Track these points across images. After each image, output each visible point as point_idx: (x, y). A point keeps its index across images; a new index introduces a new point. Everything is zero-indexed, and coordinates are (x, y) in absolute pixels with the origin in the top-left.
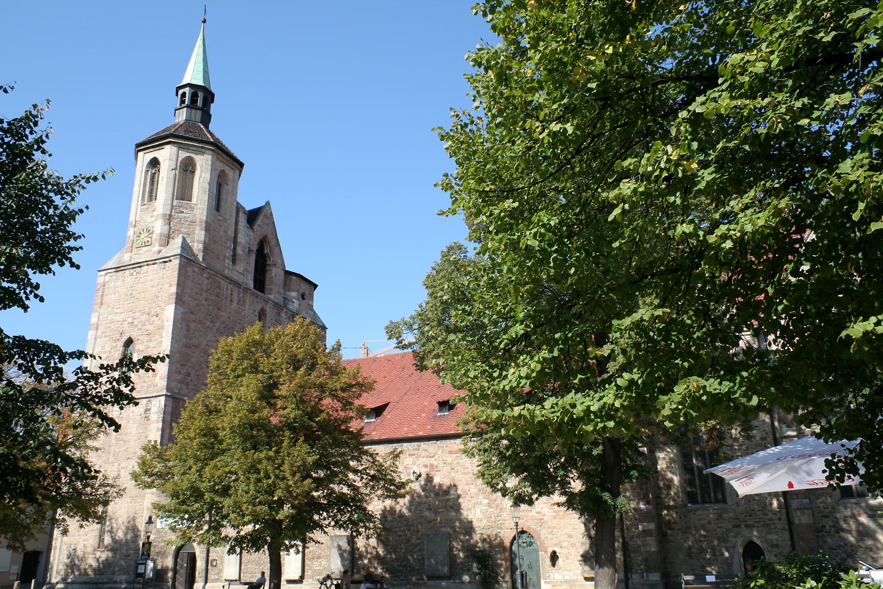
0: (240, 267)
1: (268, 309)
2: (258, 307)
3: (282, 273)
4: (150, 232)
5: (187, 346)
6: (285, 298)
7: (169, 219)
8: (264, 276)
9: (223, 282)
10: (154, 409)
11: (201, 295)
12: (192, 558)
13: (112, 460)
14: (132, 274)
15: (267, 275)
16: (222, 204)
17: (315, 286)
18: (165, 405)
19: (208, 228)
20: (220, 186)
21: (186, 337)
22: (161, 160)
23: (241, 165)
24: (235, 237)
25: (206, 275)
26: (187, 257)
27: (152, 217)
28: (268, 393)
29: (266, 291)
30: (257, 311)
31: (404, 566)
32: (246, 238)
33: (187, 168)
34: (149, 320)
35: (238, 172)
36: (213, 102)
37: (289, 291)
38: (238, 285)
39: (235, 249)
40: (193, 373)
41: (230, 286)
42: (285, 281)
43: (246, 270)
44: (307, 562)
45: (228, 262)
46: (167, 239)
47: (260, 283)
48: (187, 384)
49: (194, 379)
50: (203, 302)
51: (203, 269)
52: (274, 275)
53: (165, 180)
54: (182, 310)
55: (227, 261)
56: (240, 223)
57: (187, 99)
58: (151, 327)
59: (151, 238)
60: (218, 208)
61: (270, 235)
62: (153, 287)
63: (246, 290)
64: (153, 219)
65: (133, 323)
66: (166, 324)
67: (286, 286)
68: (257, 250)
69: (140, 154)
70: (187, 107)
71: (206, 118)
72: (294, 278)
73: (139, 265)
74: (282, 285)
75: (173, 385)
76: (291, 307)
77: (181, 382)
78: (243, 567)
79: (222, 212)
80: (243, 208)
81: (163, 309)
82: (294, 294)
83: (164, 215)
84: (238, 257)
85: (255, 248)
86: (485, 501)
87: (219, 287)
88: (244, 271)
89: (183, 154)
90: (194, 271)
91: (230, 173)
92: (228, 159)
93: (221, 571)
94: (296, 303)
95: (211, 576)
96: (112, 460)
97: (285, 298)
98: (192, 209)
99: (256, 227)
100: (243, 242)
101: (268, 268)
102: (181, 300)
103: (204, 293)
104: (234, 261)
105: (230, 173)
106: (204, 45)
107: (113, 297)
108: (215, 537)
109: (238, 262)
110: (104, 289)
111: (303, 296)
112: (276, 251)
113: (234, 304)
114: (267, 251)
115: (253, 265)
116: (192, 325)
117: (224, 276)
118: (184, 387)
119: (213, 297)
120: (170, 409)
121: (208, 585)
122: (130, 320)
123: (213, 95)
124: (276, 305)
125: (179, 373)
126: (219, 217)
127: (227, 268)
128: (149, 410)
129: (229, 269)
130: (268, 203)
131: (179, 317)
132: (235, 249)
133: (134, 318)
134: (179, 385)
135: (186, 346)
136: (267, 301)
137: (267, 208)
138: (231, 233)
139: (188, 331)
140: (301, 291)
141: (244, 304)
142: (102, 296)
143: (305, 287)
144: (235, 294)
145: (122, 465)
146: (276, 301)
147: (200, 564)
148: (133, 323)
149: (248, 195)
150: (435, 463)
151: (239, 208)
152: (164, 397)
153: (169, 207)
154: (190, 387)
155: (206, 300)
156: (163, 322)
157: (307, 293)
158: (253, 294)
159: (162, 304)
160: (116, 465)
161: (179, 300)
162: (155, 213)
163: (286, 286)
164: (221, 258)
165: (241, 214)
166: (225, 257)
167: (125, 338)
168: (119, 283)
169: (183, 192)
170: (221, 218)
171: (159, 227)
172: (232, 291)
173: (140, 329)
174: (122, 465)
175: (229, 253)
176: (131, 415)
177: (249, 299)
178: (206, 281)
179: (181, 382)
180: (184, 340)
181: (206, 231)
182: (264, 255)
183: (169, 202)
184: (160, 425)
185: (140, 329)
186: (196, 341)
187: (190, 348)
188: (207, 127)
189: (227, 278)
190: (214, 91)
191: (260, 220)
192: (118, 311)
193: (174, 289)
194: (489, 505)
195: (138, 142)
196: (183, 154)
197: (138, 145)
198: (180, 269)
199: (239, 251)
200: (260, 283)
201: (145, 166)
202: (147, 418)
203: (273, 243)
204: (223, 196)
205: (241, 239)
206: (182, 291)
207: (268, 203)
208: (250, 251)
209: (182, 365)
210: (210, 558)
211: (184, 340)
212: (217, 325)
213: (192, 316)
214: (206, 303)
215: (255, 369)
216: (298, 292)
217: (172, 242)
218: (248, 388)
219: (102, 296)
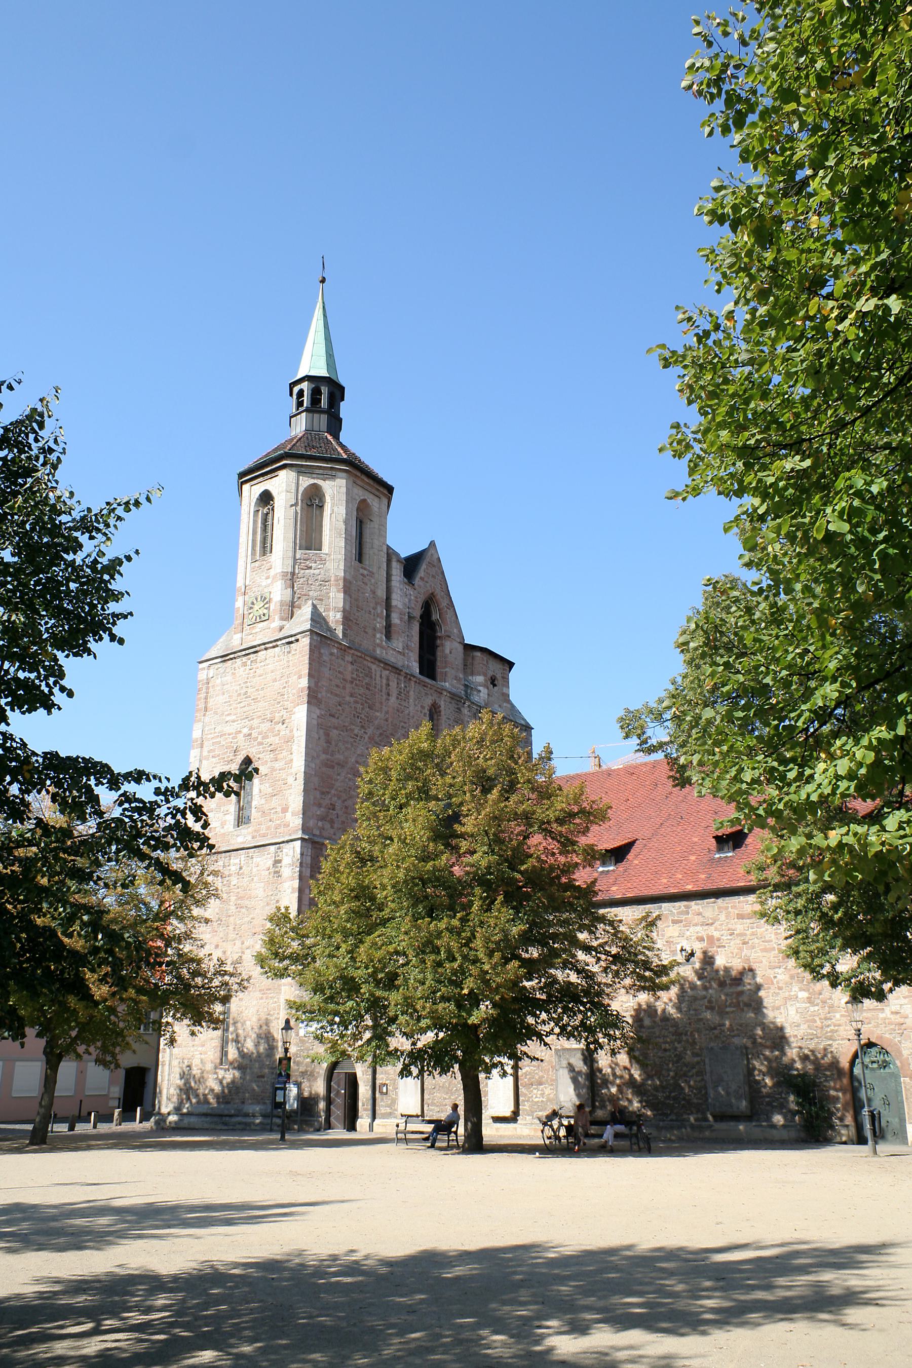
0: (398, 643)
1: (442, 704)
2: (428, 701)
3: (460, 648)
4: (266, 601)
5: (329, 764)
6: (466, 686)
7: (291, 578)
8: (434, 654)
9: (374, 667)
10: (286, 861)
11: (344, 688)
12: (352, 1082)
13: (232, 936)
14: (244, 664)
15: (439, 653)
16: (367, 550)
17: (511, 665)
18: (302, 854)
19: (347, 589)
20: (360, 524)
21: (325, 752)
22: (274, 493)
23: (390, 489)
24: (388, 599)
25: (349, 658)
26: (320, 634)
27: (268, 578)
28: (446, 830)
29: (438, 677)
30: (427, 708)
31: (675, 1098)
32: (404, 599)
33: (312, 501)
34: (272, 730)
35: (385, 501)
36: (343, 399)
37: (472, 674)
38: (396, 670)
39: (388, 616)
40: (339, 805)
41: (386, 673)
42: (465, 660)
43: (407, 647)
44: (522, 1090)
45: (380, 637)
46: (291, 609)
47: (429, 666)
48: (332, 822)
49: (340, 813)
50: (348, 698)
51: (344, 650)
52: (449, 651)
53: (282, 522)
54: (318, 712)
55: (378, 636)
56: (393, 578)
57: (305, 398)
58: (276, 740)
59: (268, 609)
60: (360, 557)
61: (439, 594)
62: (275, 680)
63: (409, 677)
64: (269, 581)
65: (250, 735)
66: (296, 734)
67: (468, 668)
68: (421, 617)
69: (246, 487)
70: (307, 410)
71: (335, 425)
72: (478, 654)
73: (253, 650)
74: (461, 666)
75: (311, 823)
76: (475, 698)
77: (322, 819)
78: (426, 1097)
79: (366, 562)
80: (397, 555)
81: (291, 713)
82: (480, 679)
83: (284, 574)
84: (393, 628)
85: (417, 613)
86: (803, 995)
87: (369, 675)
88: (404, 650)
89: (306, 482)
90: (332, 654)
91: (374, 503)
92: (371, 482)
93: (394, 1101)
94: (484, 692)
95: (380, 1110)
96: (232, 936)
97: (466, 686)
98: (323, 561)
99: (417, 581)
100: (400, 605)
101: (438, 642)
102: (316, 697)
103: (348, 686)
104: (388, 636)
105: (374, 503)
106: (325, 316)
107: (221, 699)
108: (381, 1053)
109: (394, 636)
110: (208, 688)
111: (493, 681)
112: (449, 616)
113: (393, 699)
114: (435, 616)
115: (416, 638)
116: (334, 733)
117: (376, 659)
118: (327, 826)
119: (362, 691)
120: (309, 859)
121: (377, 1121)
122: (245, 731)
123: (342, 389)
124: (454, 696)
125: (320, 805)
126: (362, 571)
127: (378, 645)
128: (280, 861)
129: (382, 647)
130: (432, 544)
131: (315, 722)
132: (388, 616)
133: (251, 728)
134: (320, 824)
135: (327, 766)
136: (440, 692)
137: (432, 551)
138: (381, 593)
139: (328, 742)
140: (490, 674)
141: (407, 697)
142: (206, 698)
143: (495, 668)
144: (393, 684)
145: (247, 944)
146: (454, 690)
147: (364, 1091)
148: (250, 735)
149: (402, 535)
150: (716, 934)
151: (391, 554)
152: (298, 844)
153: (290, 562)
154: (336, 826)
155: (352, 695)
156: (291, 731)
157: (499, 676)
158: (419, 682)
159: (288, 705)
160: (238, 943)
161: (313, 697)
162: (272, 573)
163: (468, 668)
164: (370, 631)
165: (395, 564)
166: (374, 629)
167: (240, 758)
168: (229, 678)
169: (309, 538)
170: (365, 572)
171: (278, 593)
172: (388, 679)
173: (261, 744)
174: (247, 944)
175: (380, 624)
176: (254, 870)
177: (413, 691)
178: (350, 667)
179: (322, 819)
180: (323, 756)
181: (345, 592)
182: (432, 624)
183: (291, 554)
184: (296, 883)
185: (261, 744)
186: (341, 757)
187: (333, 767)
188: (336, 437)
189: (380, 661)
190: (343, 383)
191: (422, 572)
192: (228, 718)
193: (304, 682)
194: (809, 1000)
195: (242, 469)
196: (306, 482)
197: (241, 475)
198: (311, 651)
199: (395, 619)
200: (429, 666)
201: (253, 504)
202: (277, 874)
203: (444, 603)
204: (367, 538)
205: (397, 601)
206: (316, 684)
207: (432, 544)
208: (411, 618)
209: (323, 793)
210: (378, 1082)
211: (323, 756)
212: (369, 732)
213: (334, 720)
214: (352, 700)
215: (424, 793)
216: (485, 675)
217: (297, 612)
218: (416, 823)
219: (206, 698)
